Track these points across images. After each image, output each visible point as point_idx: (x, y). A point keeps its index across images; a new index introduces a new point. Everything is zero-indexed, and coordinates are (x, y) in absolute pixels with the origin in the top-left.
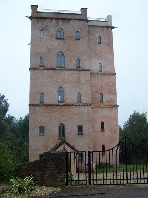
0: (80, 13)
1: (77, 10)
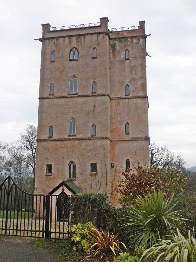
0: (99, 24)
1: (97, 22)
